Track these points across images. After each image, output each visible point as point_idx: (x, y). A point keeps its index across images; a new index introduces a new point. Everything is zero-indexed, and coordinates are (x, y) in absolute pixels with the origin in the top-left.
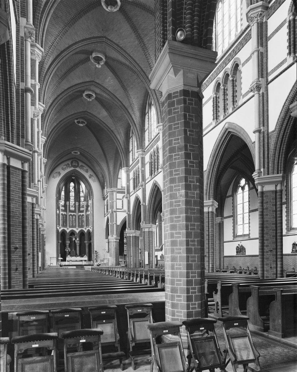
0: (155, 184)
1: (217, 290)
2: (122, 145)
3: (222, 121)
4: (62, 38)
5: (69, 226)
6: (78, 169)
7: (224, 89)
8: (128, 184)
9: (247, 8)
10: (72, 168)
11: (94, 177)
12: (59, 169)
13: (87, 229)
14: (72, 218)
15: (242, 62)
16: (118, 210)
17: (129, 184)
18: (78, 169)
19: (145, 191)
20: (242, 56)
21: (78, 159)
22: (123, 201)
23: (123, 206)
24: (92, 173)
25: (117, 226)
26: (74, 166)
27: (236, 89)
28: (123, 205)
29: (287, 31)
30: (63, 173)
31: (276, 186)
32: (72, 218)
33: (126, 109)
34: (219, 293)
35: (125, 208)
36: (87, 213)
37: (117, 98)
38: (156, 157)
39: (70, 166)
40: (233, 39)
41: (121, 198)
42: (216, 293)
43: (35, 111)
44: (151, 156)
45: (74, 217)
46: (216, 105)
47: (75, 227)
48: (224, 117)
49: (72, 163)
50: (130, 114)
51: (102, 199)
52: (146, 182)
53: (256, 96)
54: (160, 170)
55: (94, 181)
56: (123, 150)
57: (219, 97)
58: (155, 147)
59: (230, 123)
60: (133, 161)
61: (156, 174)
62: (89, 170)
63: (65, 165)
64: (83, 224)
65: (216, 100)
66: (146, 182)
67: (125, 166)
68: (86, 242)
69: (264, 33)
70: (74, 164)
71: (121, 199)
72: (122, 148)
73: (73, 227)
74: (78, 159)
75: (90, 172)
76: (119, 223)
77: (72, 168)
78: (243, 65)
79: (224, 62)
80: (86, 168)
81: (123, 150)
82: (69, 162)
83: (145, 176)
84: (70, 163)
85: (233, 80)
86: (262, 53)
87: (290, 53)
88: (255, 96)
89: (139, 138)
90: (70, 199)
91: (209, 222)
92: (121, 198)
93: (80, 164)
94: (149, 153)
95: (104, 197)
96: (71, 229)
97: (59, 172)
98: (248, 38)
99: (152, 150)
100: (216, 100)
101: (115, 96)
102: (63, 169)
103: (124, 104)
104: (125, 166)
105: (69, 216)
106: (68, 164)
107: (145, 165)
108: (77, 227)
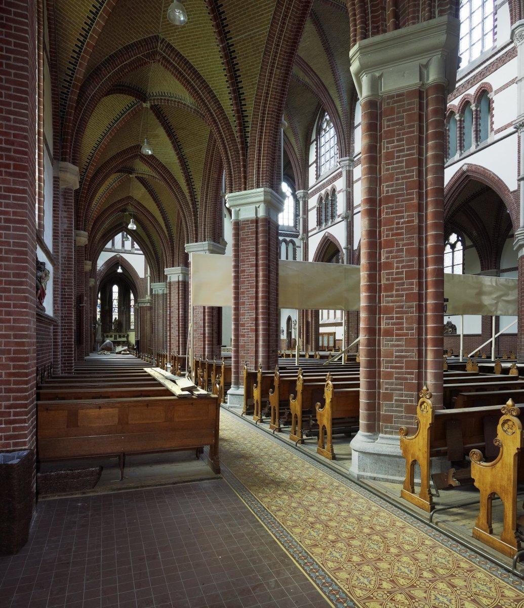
1: (325, 400)
2: (297, 154)
3: (458, 161)
7: (326, 204)
8: (305, 217)
9: (512, 23)
15: (494, 89)
17: (307, 217)
19: (353, 226)
20: (495, 80)
27: (481, 122)
33: (326, 88)
34: (299, 396)
37: (312, 70)
42: (322, 406)
44: (321, 199)
48: (325, 226)
50: (331, 98)
52: (355, 212)
54: (338, 220)
56: (298, 162)
57: (480, 111)
58: (329, 188)
59: (468, 164)
61: (329, 224)
66: (355, 212)
67: (301, 187)
68: (431, 268)
69: (351, 179)
72: (297, 158)
78: (497, 92)
79: (468, 82)
81: (298, 162)
83: (353, 201)
85: (332, 200)
86: (349, 192)
89: (344, 139)
91: (179, 330)
99: (323, 192)
101: (309, 66)
103: (323, 80)
104: (301, 187)
107: (353, 184)
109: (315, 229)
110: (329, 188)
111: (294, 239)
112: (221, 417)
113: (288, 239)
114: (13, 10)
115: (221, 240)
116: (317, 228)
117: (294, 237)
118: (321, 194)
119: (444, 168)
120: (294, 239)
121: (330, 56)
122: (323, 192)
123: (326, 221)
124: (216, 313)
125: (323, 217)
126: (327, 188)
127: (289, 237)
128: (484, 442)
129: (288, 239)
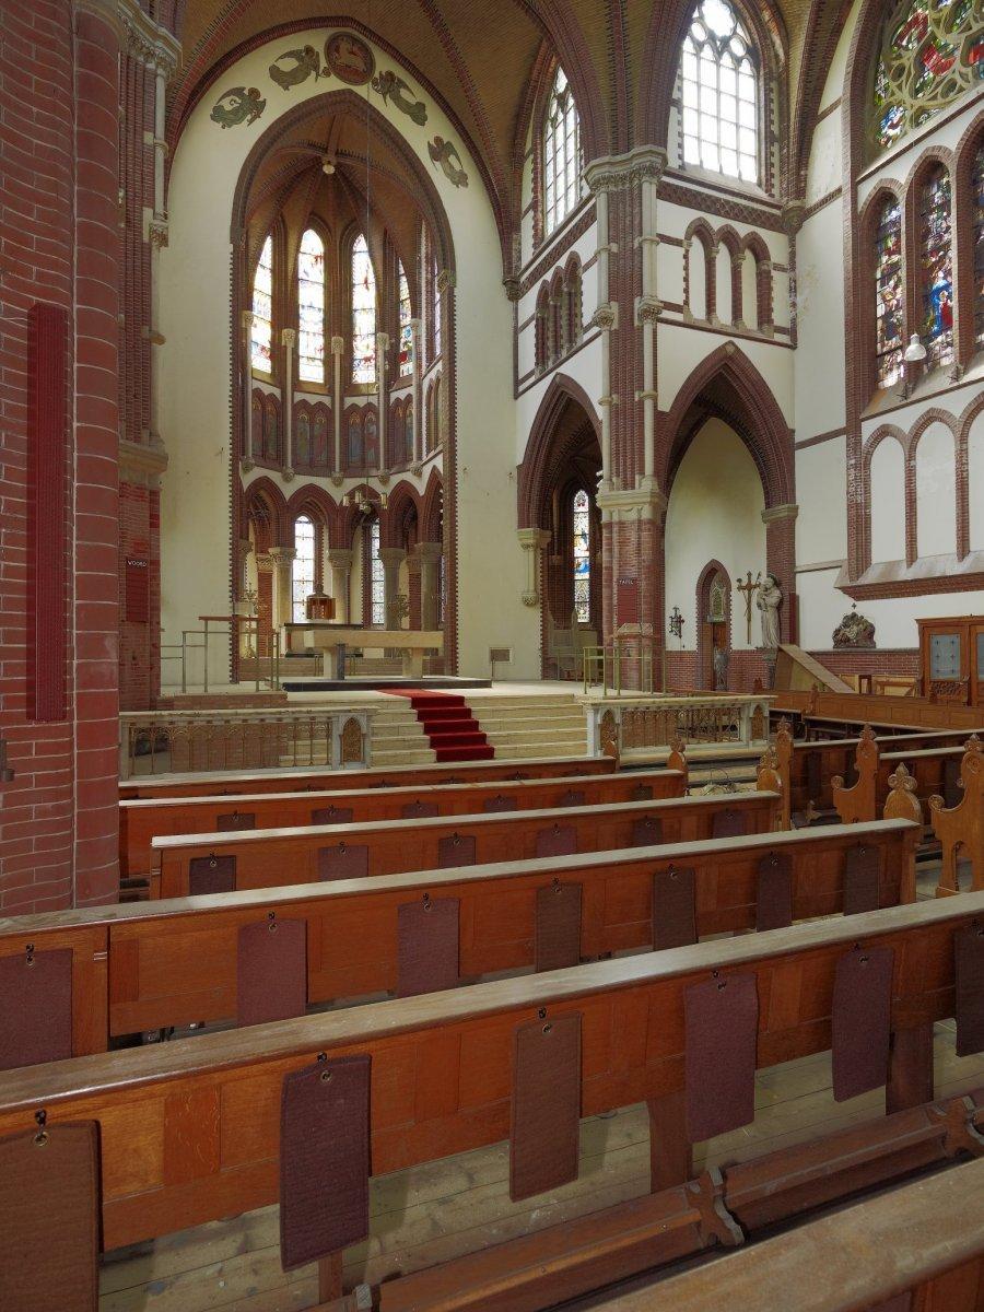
0: (558, 387)
4: (227, 28)
5: (296, 464)
6: (363, 90)
10: (333, 84)
11: (462, 161)
12: (251, 73)
13: (395, 480)
14: (312, 422)
16: (666, 314)
18: (363, 90)
21: (365, 29)
22: (686, 257)
23: (686, 291)
24: (448, 134)
25: (659, 416)
26: (345, 73)
28: (686, 280)
29: (534, 331)
30: (278, 103)
31: (639, 511)
32: (312, 422)
35: (698, 310)
36: (394, 396)
38: (552, 310)
39: (323, 64)
40: (572, 206)
41: (681, 236)
43: (152, 221)
45: (321, 418)
46: (543, 334)
47: (327, 469)
48: (568, 351)
49: (332, 47)
51: (502, 292)
53: (605, 334)
55: (459, 180)
58: (562, 262)
60: (535, 246)
61: (564, 354)
62: (433, 112)
63: (290, 54)
64: (370, 455)
65: (543, 324)
70: (345, 58)
71: (678, 243)
73: (311, 468)
74: (365, 29)
75: (437, 126)
76: (665, 405)
77: (333, 84)
80: (415, 94)
82: (317, 40)
84: (319, 48)
85: (555, 307)
87: (537, 364)
88: (604, 333)
90: (297, 317)
92: (681, 236)
93: (383, 64)
94: (538, 285)
95: (515, 282)
96: (302, 481)
97: (254, 93)
98: (591, 218)
99: (548, 276)
100: (543, 324)
102: (284, 79)
105: (294, 406)
106: (309, 50)
108: (337, 474)
109: (532, 373)
110: (562, 262)
111: (766, 235)
112: (270, 287)
113: (742, 229)
114: (35, 268)
115: (145, 435)
116: (537, 372)
117: (763, 226)
118: (545, 281)
119: (807, 213)
120: (766, 235)
121: (617, 16)
122: (548, 276)
123: (557, 350)
124: (6, 699)
125: (550, 343)
126: (544, 277)
127: (745, 220)
128: (124, 810)
129: (742, 229)
